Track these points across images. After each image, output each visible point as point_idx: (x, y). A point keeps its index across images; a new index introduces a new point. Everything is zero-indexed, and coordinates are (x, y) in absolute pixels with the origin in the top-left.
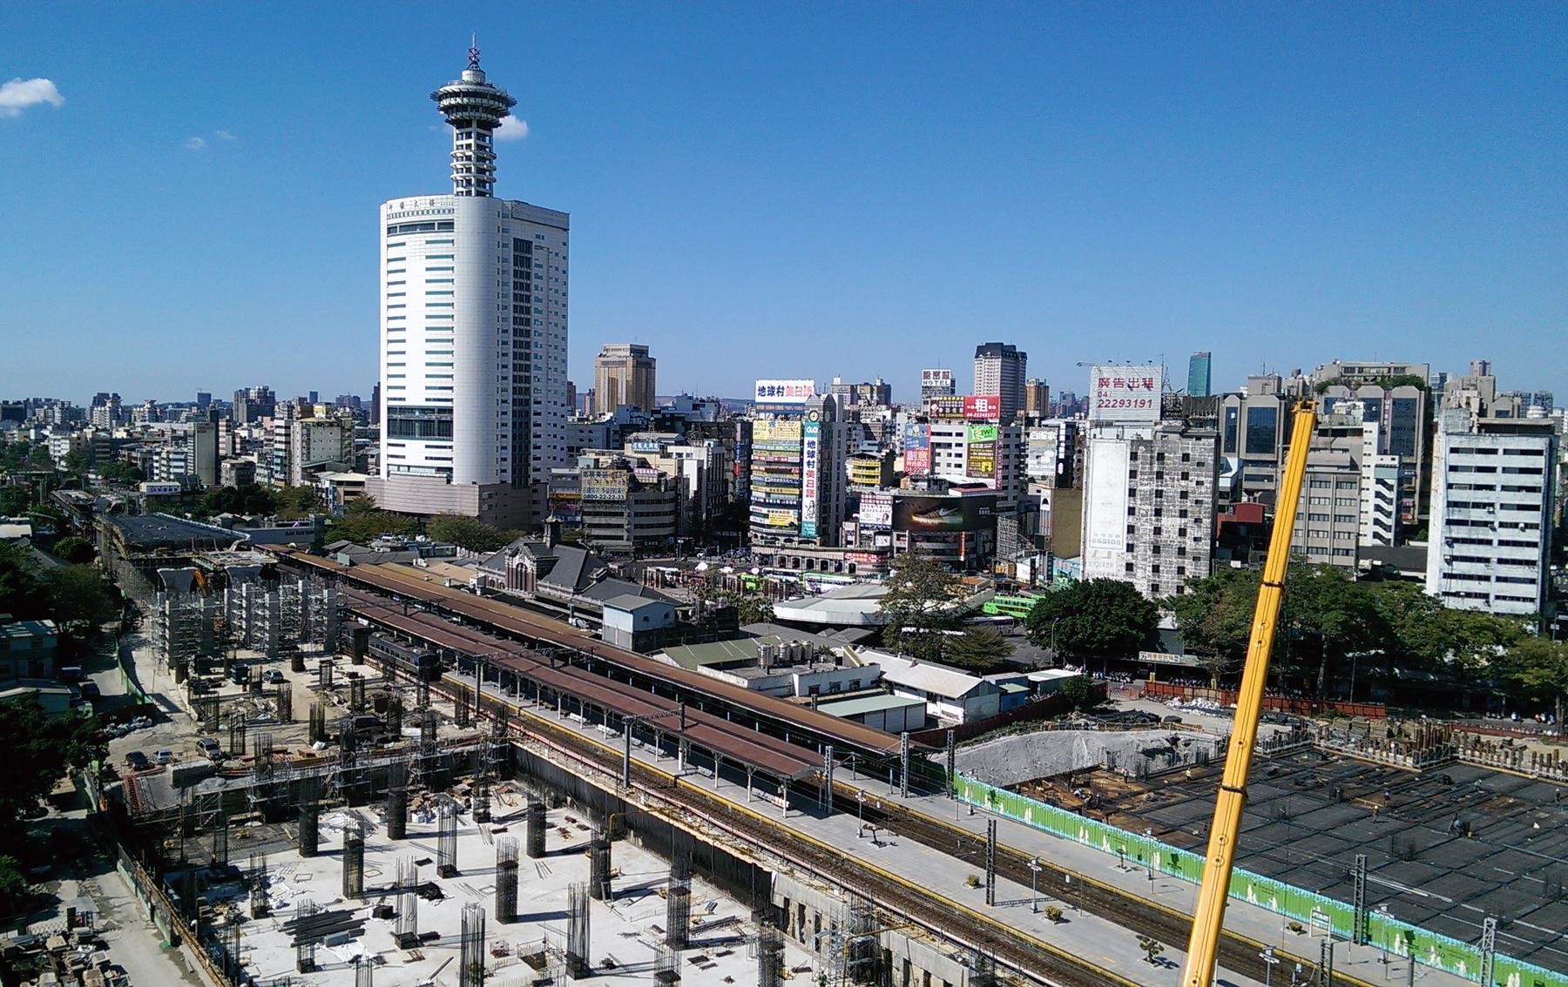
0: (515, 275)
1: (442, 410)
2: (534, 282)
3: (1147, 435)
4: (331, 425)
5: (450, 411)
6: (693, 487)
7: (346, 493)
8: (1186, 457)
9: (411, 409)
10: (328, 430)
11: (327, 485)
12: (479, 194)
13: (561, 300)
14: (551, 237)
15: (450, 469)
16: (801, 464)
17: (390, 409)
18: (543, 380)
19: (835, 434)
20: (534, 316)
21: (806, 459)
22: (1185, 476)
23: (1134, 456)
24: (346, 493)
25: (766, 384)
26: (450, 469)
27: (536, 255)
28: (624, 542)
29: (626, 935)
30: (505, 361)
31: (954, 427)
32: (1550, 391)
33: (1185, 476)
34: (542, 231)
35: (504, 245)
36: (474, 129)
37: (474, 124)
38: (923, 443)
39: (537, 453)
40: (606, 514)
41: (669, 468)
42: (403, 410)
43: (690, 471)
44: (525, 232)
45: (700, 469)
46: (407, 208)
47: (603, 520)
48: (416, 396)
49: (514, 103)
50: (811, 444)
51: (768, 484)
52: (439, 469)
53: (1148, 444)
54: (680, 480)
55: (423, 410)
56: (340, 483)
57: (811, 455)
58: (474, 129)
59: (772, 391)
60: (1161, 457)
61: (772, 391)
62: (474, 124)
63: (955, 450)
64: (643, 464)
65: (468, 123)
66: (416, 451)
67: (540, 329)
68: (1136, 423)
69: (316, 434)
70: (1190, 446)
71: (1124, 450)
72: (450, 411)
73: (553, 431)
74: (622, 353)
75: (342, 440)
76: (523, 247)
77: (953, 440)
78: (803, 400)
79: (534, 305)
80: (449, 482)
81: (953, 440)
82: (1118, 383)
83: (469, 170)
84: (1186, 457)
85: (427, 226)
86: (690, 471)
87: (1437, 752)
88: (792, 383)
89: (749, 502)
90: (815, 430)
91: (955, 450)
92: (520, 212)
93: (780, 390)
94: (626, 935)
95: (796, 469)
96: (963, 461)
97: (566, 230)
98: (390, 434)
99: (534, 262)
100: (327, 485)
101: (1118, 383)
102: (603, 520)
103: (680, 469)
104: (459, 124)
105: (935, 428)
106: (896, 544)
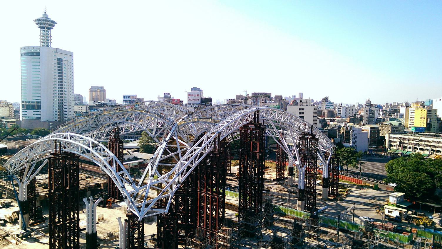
0: (58, 67)
1: (38, 102)
2: (64, 92)
7: (10, 125)
11: (5, 122)
13: (72, 83)
18: (67, 94)
20: (64, 78)
24: (10, 125)
26: (40, 118)
27: (64, 62)
30: (55, 80)
34: (66, 56)
35: (55, 60)
36: (45, 29)
37: (45, 28)
39: (66, 107)
52: (37, 118)
56: (8, 122)
58: (45, 29)
62: (45, 28)
65: (44, 28)
67: (66, 81)
75: (9, 111)
76: (60, 61)
79: (64, 75)
83: (44, 43)
87: (301, 144)
89: (185, 233)
97: (73, 56)
100: (5, 122)
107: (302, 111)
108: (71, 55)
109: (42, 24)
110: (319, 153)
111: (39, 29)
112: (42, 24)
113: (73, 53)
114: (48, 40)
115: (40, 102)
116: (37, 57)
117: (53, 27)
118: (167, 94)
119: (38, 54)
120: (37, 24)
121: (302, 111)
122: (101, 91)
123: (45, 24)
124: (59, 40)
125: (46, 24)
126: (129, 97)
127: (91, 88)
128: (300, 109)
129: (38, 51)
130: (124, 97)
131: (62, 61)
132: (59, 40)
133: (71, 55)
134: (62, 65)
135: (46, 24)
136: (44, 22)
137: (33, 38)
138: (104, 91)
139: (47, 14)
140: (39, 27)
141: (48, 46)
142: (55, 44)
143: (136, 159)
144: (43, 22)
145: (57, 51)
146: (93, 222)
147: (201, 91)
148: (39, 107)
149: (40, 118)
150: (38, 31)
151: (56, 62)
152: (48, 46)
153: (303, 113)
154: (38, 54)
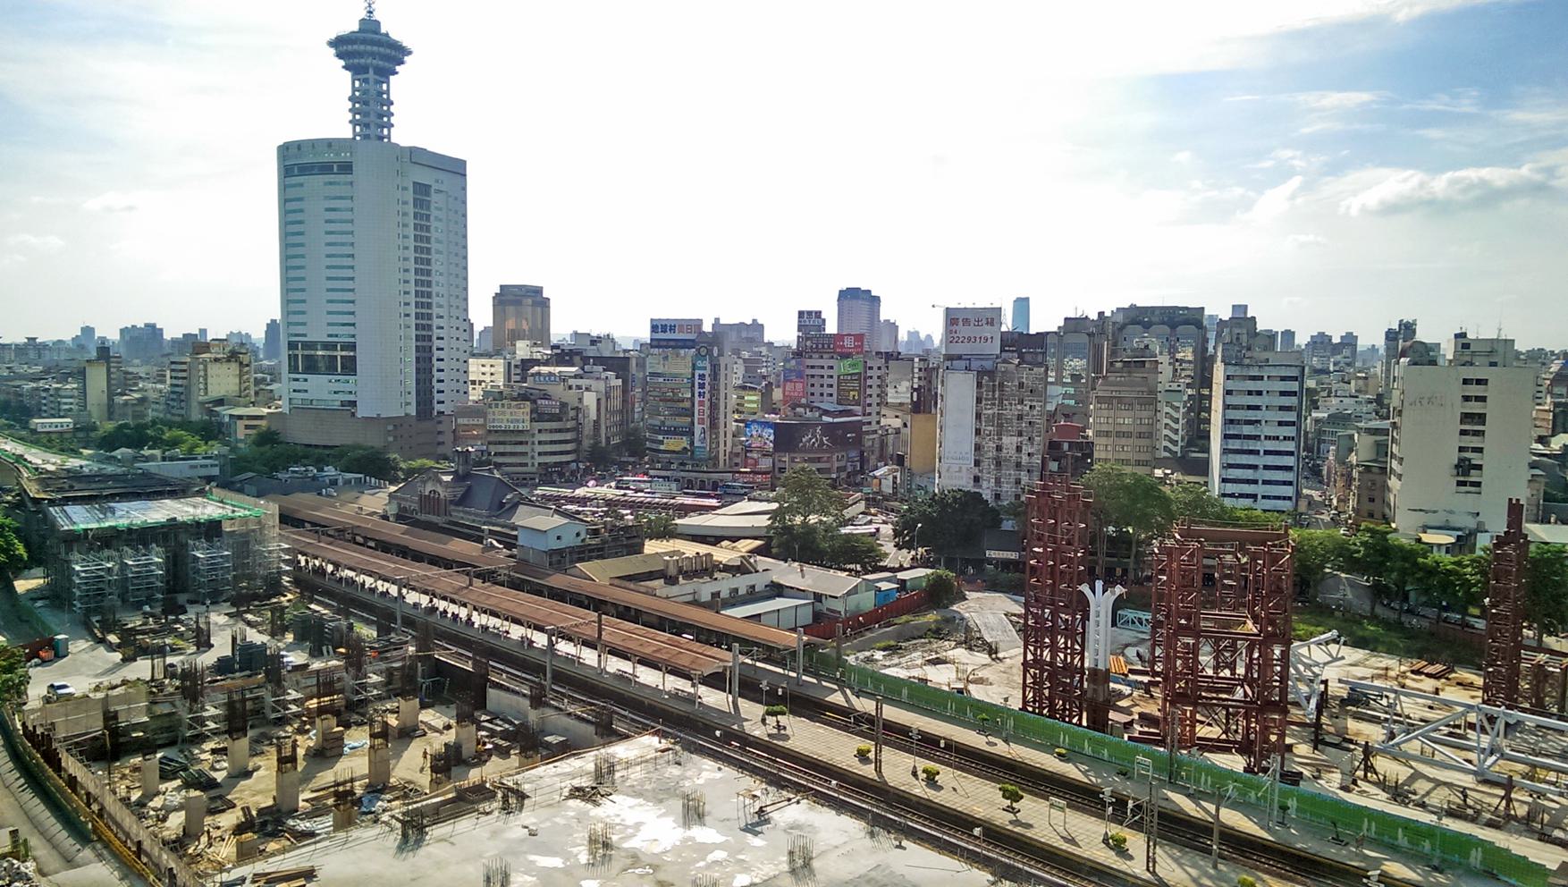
6: (593, 416)
7: (247, 427)
8: (1021, 385)
14: (447, 181)
22: (1021, 402)
23: (979, 385)
24: (247, 427)
26: (353, 404)
27: (434, 197)
36: (371, 75)
40: (511, 443)
43: (590, 400)
44: (425, 177)
49: (410, 53)
56: (240, 417)
58: (371, 75)
60: (1001, 385)
63: (827, 381)
65: (365, 69)
71: (971, 378)
75: (240, 376)
77: (825, 372)
81: (825, 372)
83: (367, 126)
85: (325, 168)
86: (590, 400)
91: (827, 381)
96: (834, 390)
98: (293, 369)
105: (809, 362)
107: (1474, 390)
108: (457, 169)
109: (360, 54)
110: (537, 362)
111: (348, 74)
112: (360, 54)
113: (464, 162)
114: (381, 116)
115: (353, 347)
116: (342, 178)
117: (398, 68)
118: (810, 313)
119: (346, 168)
120: (340, 56)
121: (1474, 390)
122: (535, 304)
123: (373, 55)
124: (417, 119)
125: (370, 55)
126: (672, 328)
127: (1260, 327)
128: (1466, 382)
129: (345, 156)
130: (654, 328)
131: (428, 194)
132: (417, 119)
133: (457, 169)
134: (428, 208)
135: (370, 55)
136: (369, 48)
137: (327, 112)
138: (545, 304)
139: (376, 16)
140: (346, 67)
141: (382, 138)
142: (402, 135)
143: (777, 590)
144: (362, 47)
145: (416, 156)
146: (403, 618)
147: (877, 299)
148: (350, 366)
149: (353, 404)
150: (340, 82)
151: (409, 196)
152: (382, 138)
153: (1483, 399)
154: (346, 168)
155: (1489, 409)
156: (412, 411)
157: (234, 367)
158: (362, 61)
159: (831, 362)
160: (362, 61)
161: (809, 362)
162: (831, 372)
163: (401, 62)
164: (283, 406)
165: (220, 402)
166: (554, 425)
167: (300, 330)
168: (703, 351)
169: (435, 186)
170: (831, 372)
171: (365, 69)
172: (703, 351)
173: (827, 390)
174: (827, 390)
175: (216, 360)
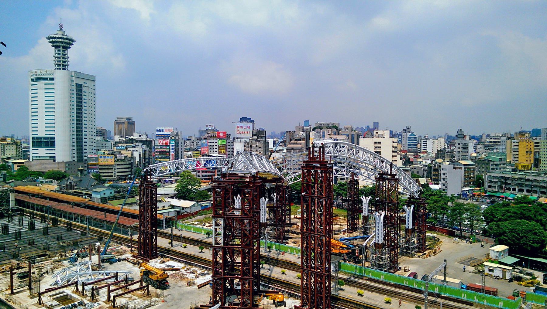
1: (51, 138)
3: (248, 140)
4: (12, 144)
5: (54, 138)
6: (137, 159)
7: (18, 166)
8: (257, 146)
9: (41, 138)
10: (11, 146)
12: (63, 69)
14: (89, 84)
15: (54, 157)
16: (170, 152)
17: (33, 138)
19: (180, 143)
21: (171, 150)
22: (257, 151)
23: (245, 146)
24: (18, 166)
25: (159, 129)
26: (54, 157)
28: (114, 177)
29: (5, 46)
31: (214, 141)
32: (408, 125)
33: (257, 151)
34: (85, 81)
36: (61, 49)
38: (206, 145)
40: (107, 169)
41: (129, 154)
42: (37, 138)
43: (136, 155)
44: (80, 82)
45: (140, 155)
46: (38, 73)
47: (106, 171)
48: (42, 133)
49: (75, 41)
50: (173, 146)
51: (160, 158)
52: (51, 157)
53: (248, 143)
54: (132, 158)
55: (45, 138)
56: (16, 163)
57: (173, 149)
58: (61, 49)
59: (161, 131)
60: (251, 146)
61: (161, 131)
63: (215, 147)
64: (120, 153)
65: (59, 47)
66: (42, 151)
68: (247, 138)
69: (7, 147)
70: (257, 143)
71: (242, 144)
72: (54, 138)
73: (91, 144)
74: (123, 120)
76: (79, 87)
77: (215, 144)
78: (170, 133)
80: (54, 161)
81: (215, 144)
82: (241, 127)
84: (257, 146)
85: (45, 79)
86: (136, 155)
88: (166, 128)
90: (173, 142)
91: (215, 147)
92: (78, 75)
93: (163, 131)
94: (5, 46)
95: (168, 153)
96: (217, 150)
98: (33, 146)
99: (83, 91)
101: (241, 127)
102: (106, 171)
103: (132, 154)
104: (56, 47)
105: (210, 141)
106: (198, 174)
107: (378, 145)
123: (62, 42)
128: (375, 143)
134: (81, 92)
154: (52, 79)
155: (381, 150)
156: (75, 159)
157: (14, 147)
158: (58, 44)
159: (216, 141)
160: (58, 44)
161: (210, 141)
162: (216, 144)
163: (72, 44)
164: (474, 301)
165: (9, 158)
166: (122, 163)
167: (36, 133)
168: (173, 138)
169: (84, 85)
170: (216, 144)
171: (59, 47)
172: (173, 138)
173: (215, 150)
174: (215, 150)
175: (8, 144)
